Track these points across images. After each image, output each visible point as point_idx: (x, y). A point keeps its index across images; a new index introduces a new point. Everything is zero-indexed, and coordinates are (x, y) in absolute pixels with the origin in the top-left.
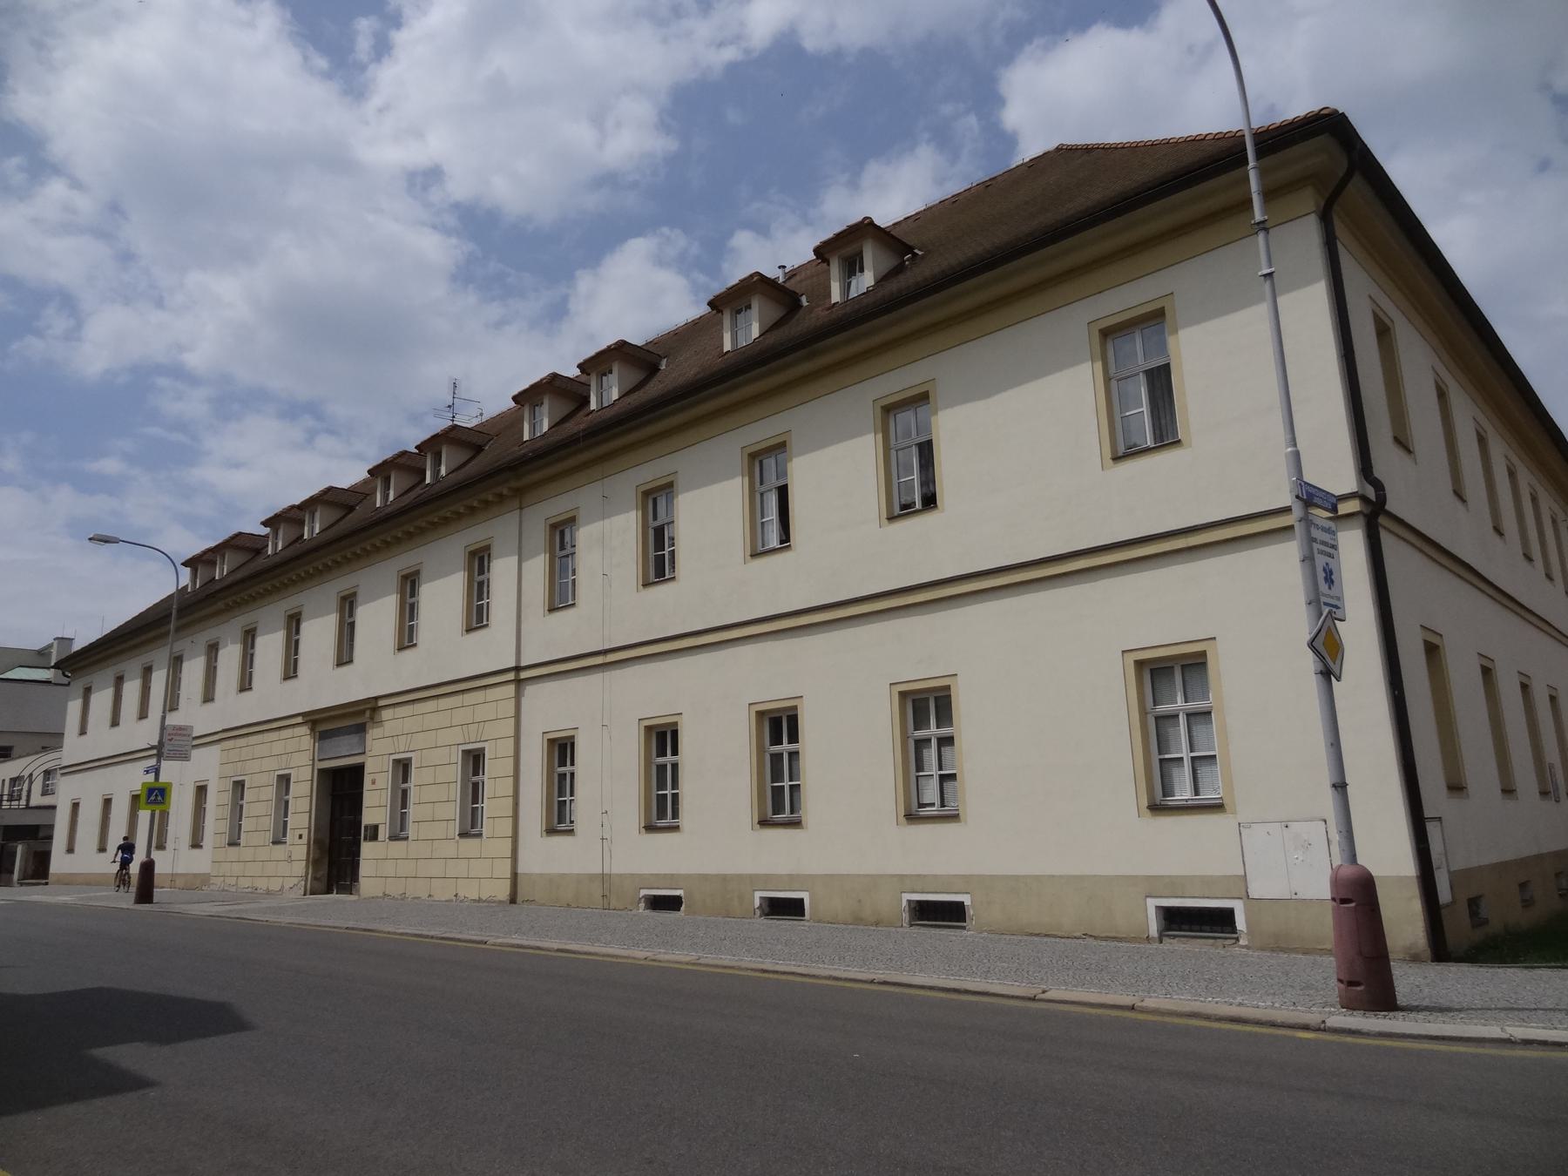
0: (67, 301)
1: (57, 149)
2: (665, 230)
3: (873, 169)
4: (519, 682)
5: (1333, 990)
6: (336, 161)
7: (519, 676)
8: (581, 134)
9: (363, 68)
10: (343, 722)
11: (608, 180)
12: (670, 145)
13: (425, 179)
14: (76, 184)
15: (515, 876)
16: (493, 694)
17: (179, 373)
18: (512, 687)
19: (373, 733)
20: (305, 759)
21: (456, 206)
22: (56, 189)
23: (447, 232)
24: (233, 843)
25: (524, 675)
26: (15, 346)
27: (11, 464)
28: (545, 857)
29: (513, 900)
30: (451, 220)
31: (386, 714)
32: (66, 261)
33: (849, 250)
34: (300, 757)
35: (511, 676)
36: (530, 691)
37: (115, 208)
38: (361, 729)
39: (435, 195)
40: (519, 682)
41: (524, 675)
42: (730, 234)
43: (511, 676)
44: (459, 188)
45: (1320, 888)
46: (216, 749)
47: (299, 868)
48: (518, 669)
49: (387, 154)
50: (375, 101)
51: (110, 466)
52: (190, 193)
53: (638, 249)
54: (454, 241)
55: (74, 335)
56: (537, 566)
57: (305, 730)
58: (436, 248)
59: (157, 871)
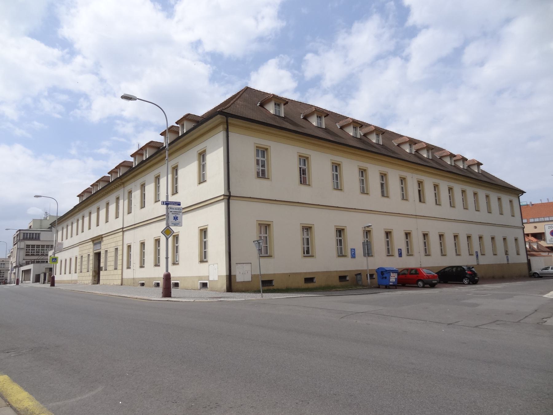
0: (86, 97)
1: (77, 46)
2: (281, 55)
3: (356, 26)
4: (123, 231)
5: (161, 295)
6: (166, 41)
7: (123, 230)
8: (250, 23)
9: (173, 7)
10: (97, 240)
11: (261, 39)
12: (284, 24)
13: (197, 44)
14: (84, 57)
15: (122, 279)
16: (117, 235)
17: (121, 118)
18: (121, 233)
19: (102, 244)
20: (91, 250)
21: (208, 54)
22: (79, 59)
23: (206, 62)
24: (81, 272)
25: (124, 229)
26: (72, 113)
27: (73, 152)
28: (128, 274)
29: (122, 285)
30: (209, 59)
31: (104, 239)
32: (85, 83)
33: (182, 123)
34: (90, 249)
35: (121, 230)
36: (125, 233)
37: (97, 64)
38: (100, 243)
39: (200, 51)
40: (123, 231)
41: (124, 229)
42: (305, 55)
43: (121, 230)
44: (208, 47)
45: (162, 276)
46: (77, 248)
47: (91, 278)
48: (123, 228)
49: (184, 37)
50: (176, 19)
51: (103, 151)
52: (121, 55)
53: (273, 62)
54: (209, 66)
55: (89, 108)
56: (126, 202)
57: (91, 243)
58: (203, 70)
59: (56, 279)
